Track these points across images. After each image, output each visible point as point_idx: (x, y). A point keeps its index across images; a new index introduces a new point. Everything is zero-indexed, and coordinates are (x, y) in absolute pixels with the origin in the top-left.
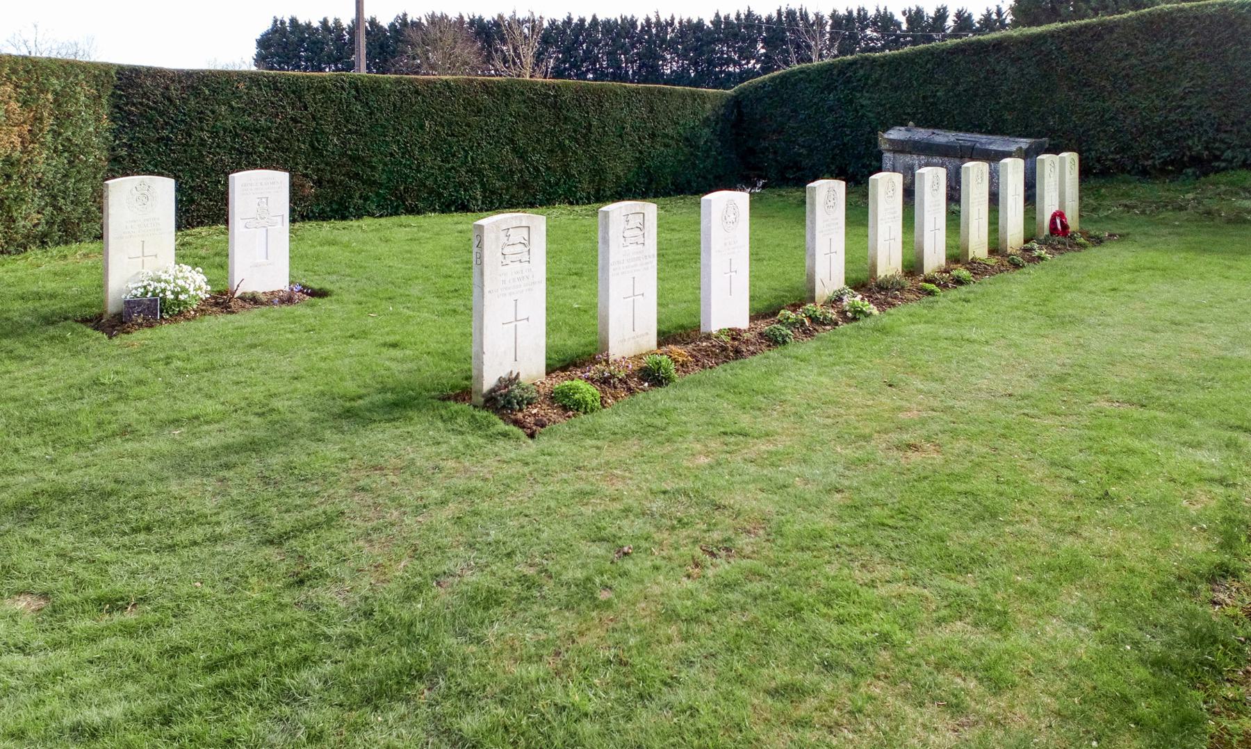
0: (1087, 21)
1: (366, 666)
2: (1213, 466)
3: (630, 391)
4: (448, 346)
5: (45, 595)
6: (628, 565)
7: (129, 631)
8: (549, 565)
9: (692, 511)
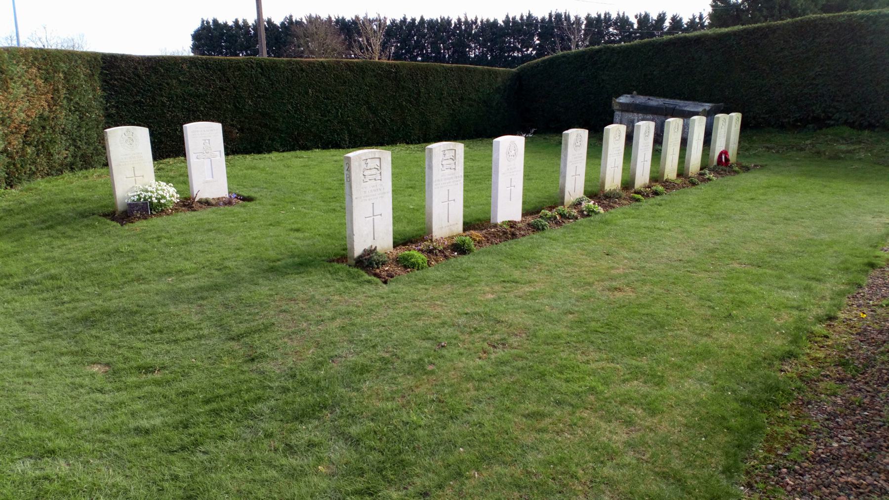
0: (759, 25)
1: (294, 402)
2: (794, 300)
3: (445, 256)
4: (332, 231)
5: (108, 364)
6: (444, 352)
7: (157, 383)
8: (398, 352)
9: (483, 324)
